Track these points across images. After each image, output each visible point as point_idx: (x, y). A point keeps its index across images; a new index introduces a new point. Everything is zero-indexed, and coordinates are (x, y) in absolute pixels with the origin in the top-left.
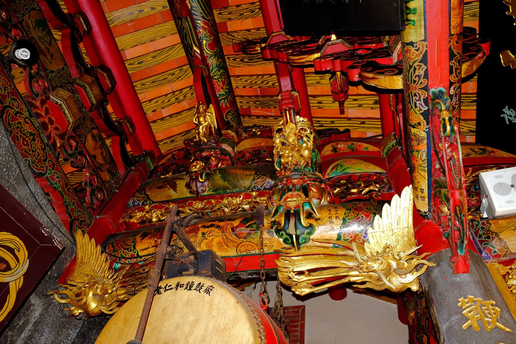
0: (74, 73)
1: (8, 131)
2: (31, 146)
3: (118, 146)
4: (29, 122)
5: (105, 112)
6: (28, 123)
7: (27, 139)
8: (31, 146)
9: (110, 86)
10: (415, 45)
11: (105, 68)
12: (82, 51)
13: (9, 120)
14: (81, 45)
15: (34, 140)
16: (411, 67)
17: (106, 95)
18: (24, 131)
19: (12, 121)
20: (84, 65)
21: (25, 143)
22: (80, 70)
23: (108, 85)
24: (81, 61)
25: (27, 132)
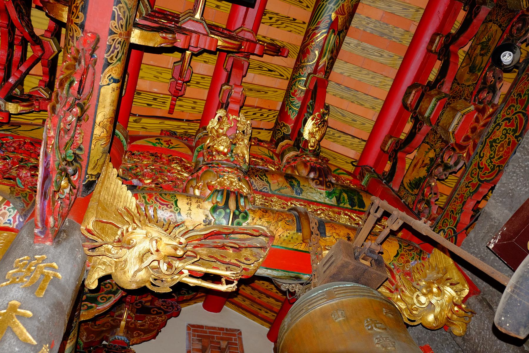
0: (425, 128)
1: (500, 171)
2: (501, 141)
3: (461, 39)
4: (482, 153)
5: (439, 77)
6: (484, 154)
7: (497, 148)
8: (501, 141)
9: (414, 92)
10: (112, 80)
11: (404, 105)
12: (459, 25)
13: (489, 173)
14: (453, 31)
15: (495, 141)
16: (119, 60)
17: (424, 89)
18: (492, 154)
19: (488, 170)
20: (414, 127)
21: (501, 149)
22: (478, 10)
23: (415, 94)
24: (468, 17)
25: (492, 151)
